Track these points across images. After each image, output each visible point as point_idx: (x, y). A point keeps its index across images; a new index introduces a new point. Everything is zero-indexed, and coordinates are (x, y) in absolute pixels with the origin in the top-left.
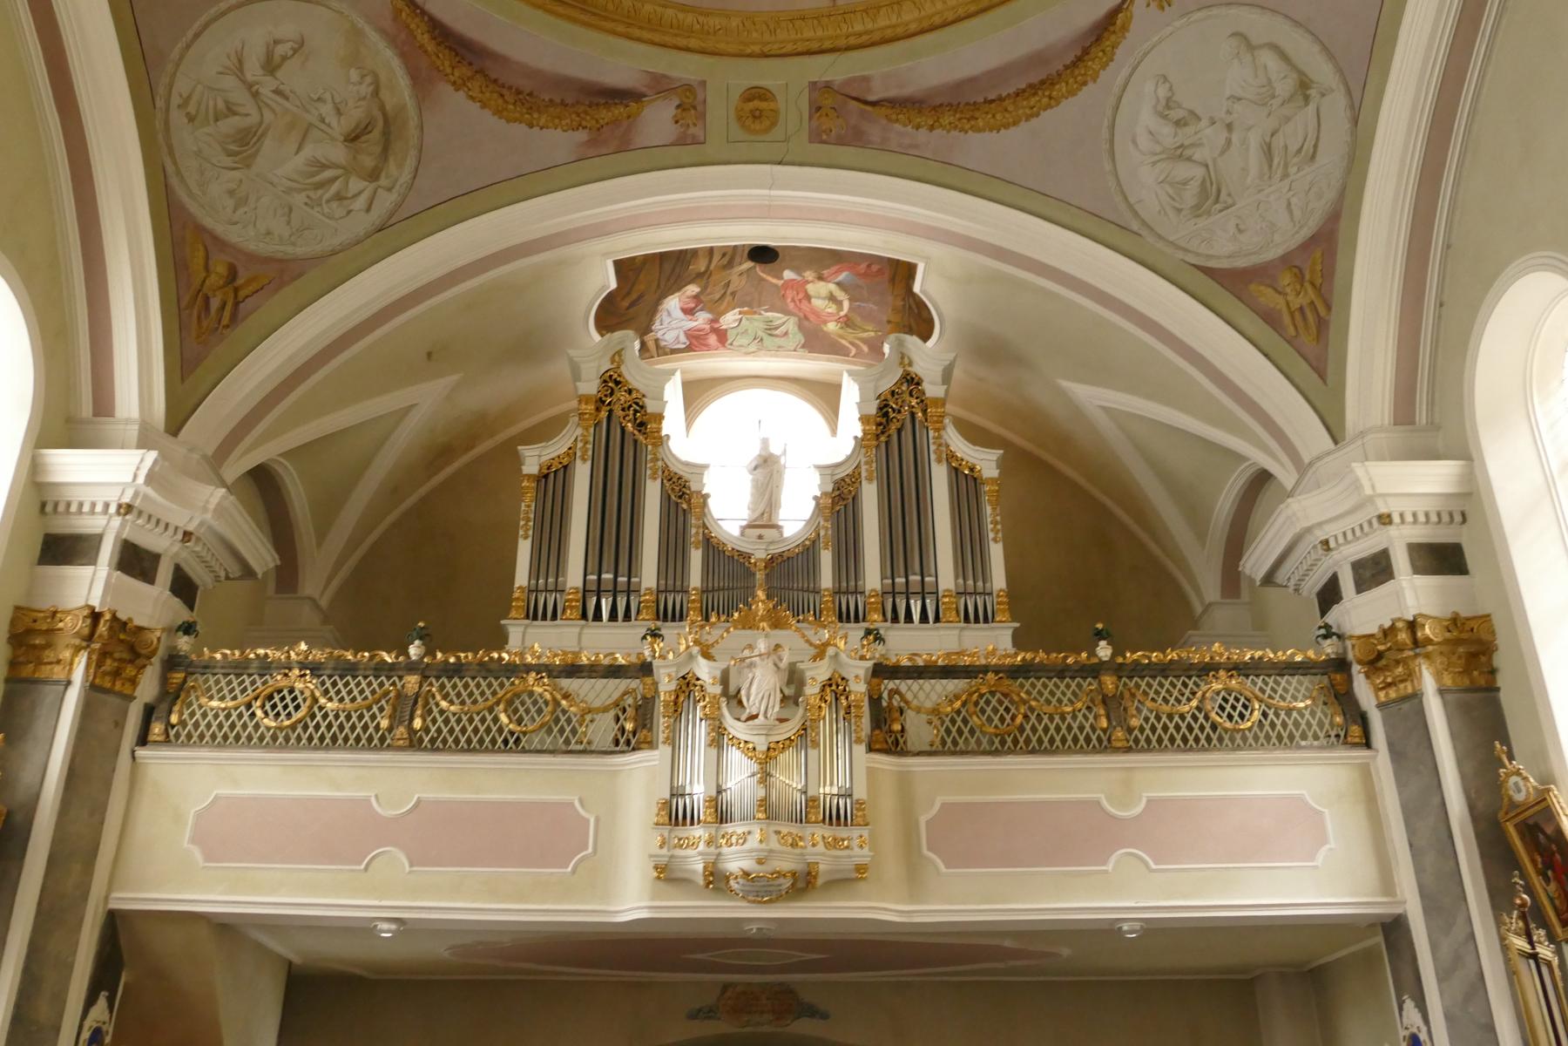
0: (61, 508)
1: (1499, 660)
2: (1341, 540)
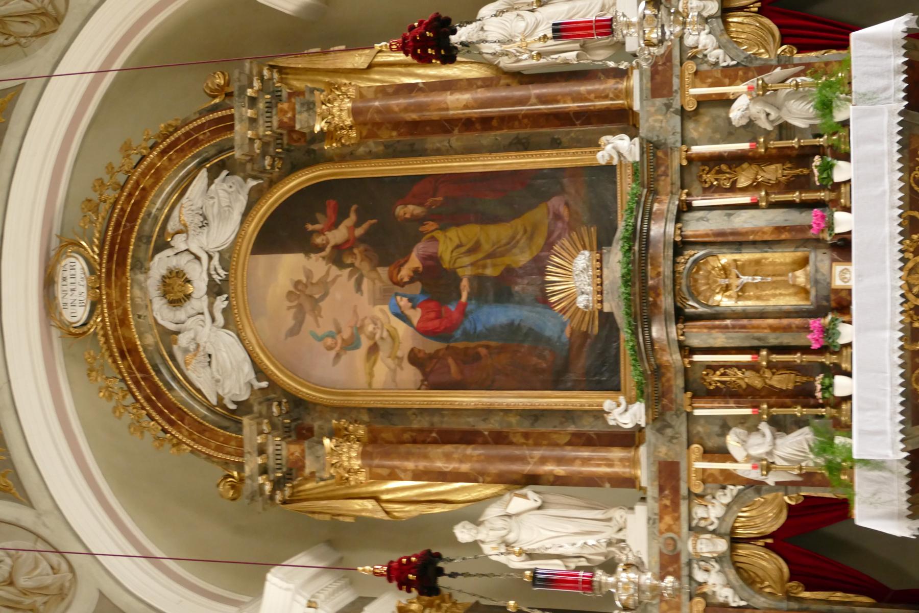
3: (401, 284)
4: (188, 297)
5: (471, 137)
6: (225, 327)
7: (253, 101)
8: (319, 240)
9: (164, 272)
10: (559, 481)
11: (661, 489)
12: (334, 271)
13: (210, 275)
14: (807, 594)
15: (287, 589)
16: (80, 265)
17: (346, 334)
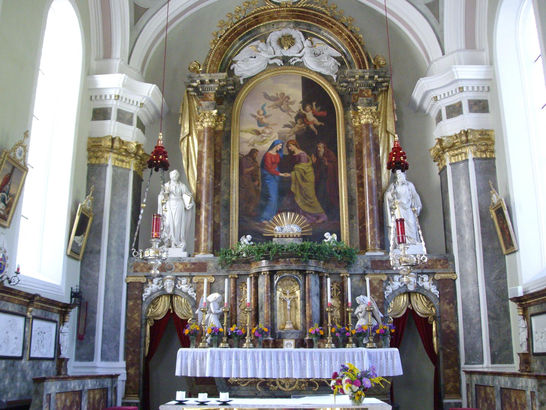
0: (103, 98)
1: (496, 147)
2: (442, 97)
4: (282, 47)
5: (355, 178)
6: (268, 64)
7: (371, 78)
8: (308, 108)
9: (294, 36)
11: (194, 264)
12: (294, 115)
13: (292, 57)
17: (265, 120)
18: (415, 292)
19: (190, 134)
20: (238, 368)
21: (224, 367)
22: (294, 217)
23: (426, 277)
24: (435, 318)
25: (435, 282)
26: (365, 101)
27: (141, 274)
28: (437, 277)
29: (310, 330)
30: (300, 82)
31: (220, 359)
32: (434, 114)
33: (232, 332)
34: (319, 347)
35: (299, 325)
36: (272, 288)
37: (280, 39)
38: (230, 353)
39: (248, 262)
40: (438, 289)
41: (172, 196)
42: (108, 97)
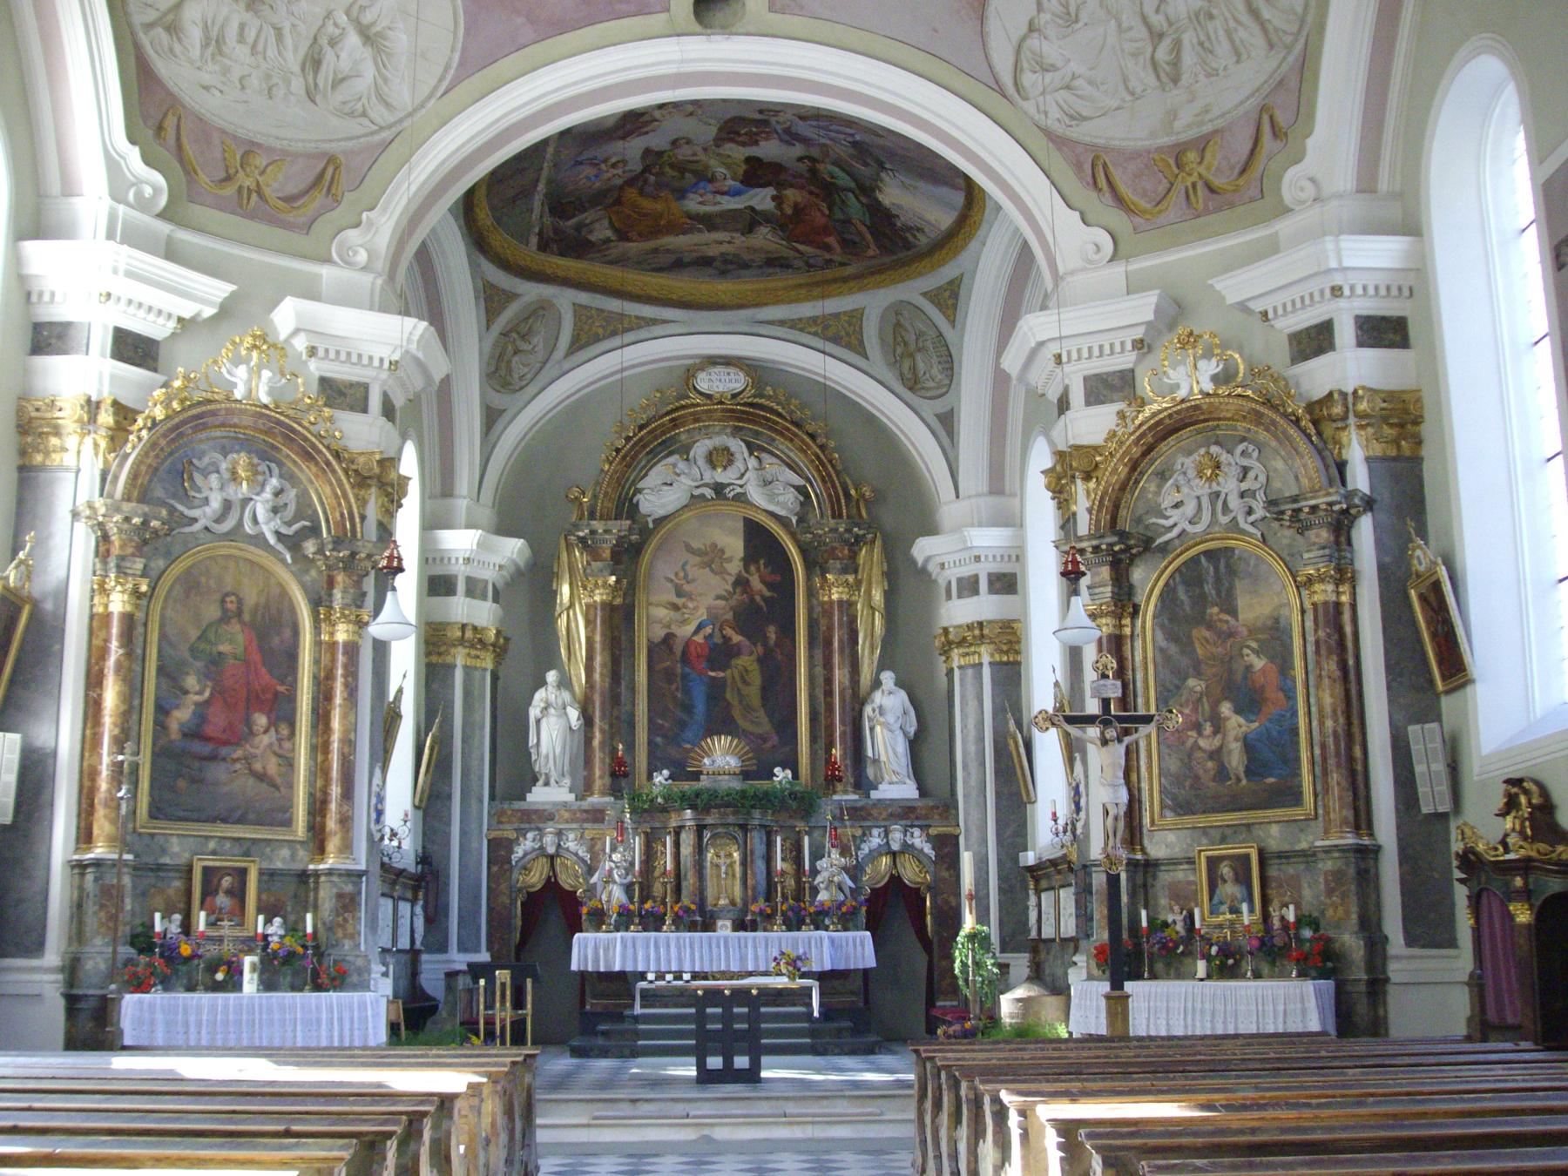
0: (446, 561)
1: (1426, 429)
3: (721, 630)
4: (714, 467)
5: (820, 681)
6: (692, 496)
7: (848, 531)
8: (752, 568)
9: (733, 449)
10: (588, 741)
11: (586, 811)
12: (731, 579)
13: (729, 484)
14: (519, 903)
15: (409, 340)
16: (738, 387)
17: (687, 588)
18: (902, 852)
19: (572, 605)
20: (658, 959)
21: (640, 958)
22: (731, 742)
23: (917, 832)
24: (929, 888)
25: (929, 839)
26: (838, 566)
27: (508, 826)
28: (933, 831)
29: (753, 908)
30: (741, 524)
31: (634, 946)
32: (942, 583)
33: (647, 911)
34: (765, 930)
35: (738, 900)
36: (700, 849)
37: (710, 454)
38: (648, 940)
39: (664, 810)
40: (933, 849)
41: (552, 711)
42: (453, 561)
